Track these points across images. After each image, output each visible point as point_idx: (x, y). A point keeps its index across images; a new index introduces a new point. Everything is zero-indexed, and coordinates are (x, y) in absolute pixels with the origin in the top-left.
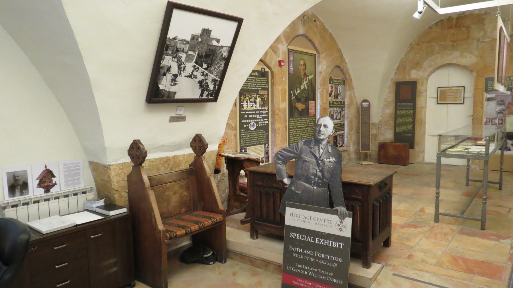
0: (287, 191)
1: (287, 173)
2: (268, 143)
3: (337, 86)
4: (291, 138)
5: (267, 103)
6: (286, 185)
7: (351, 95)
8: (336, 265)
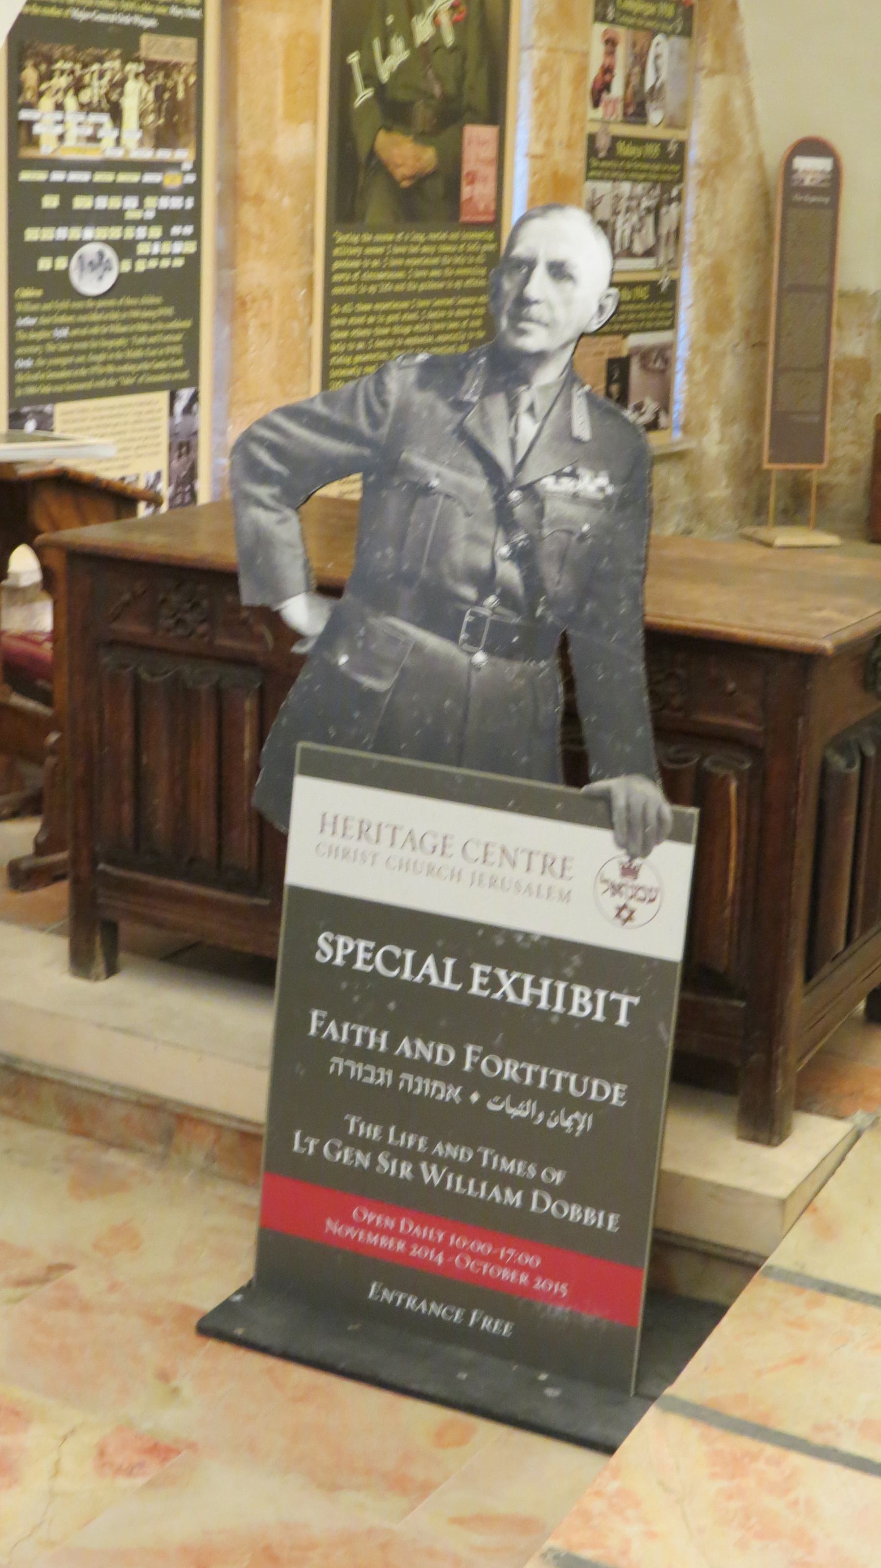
0: (304, 677)
1: (307, 562)
2: (194, 381)
3: (642, 36)
4: (339, 360)
5: (193, 124)
6: (297, 636)
7: (725, 101)
8: (583, 1121)
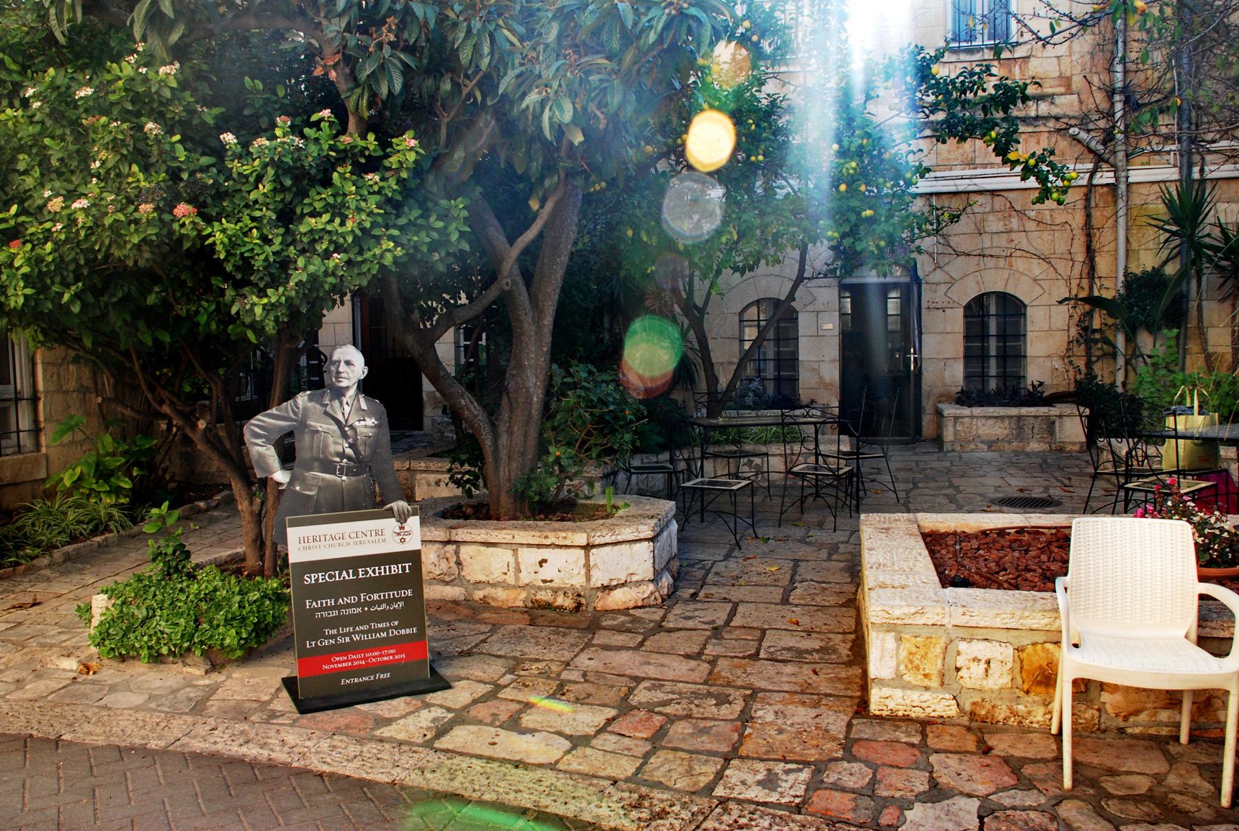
6: (279, 484)
8: (401, 604)
